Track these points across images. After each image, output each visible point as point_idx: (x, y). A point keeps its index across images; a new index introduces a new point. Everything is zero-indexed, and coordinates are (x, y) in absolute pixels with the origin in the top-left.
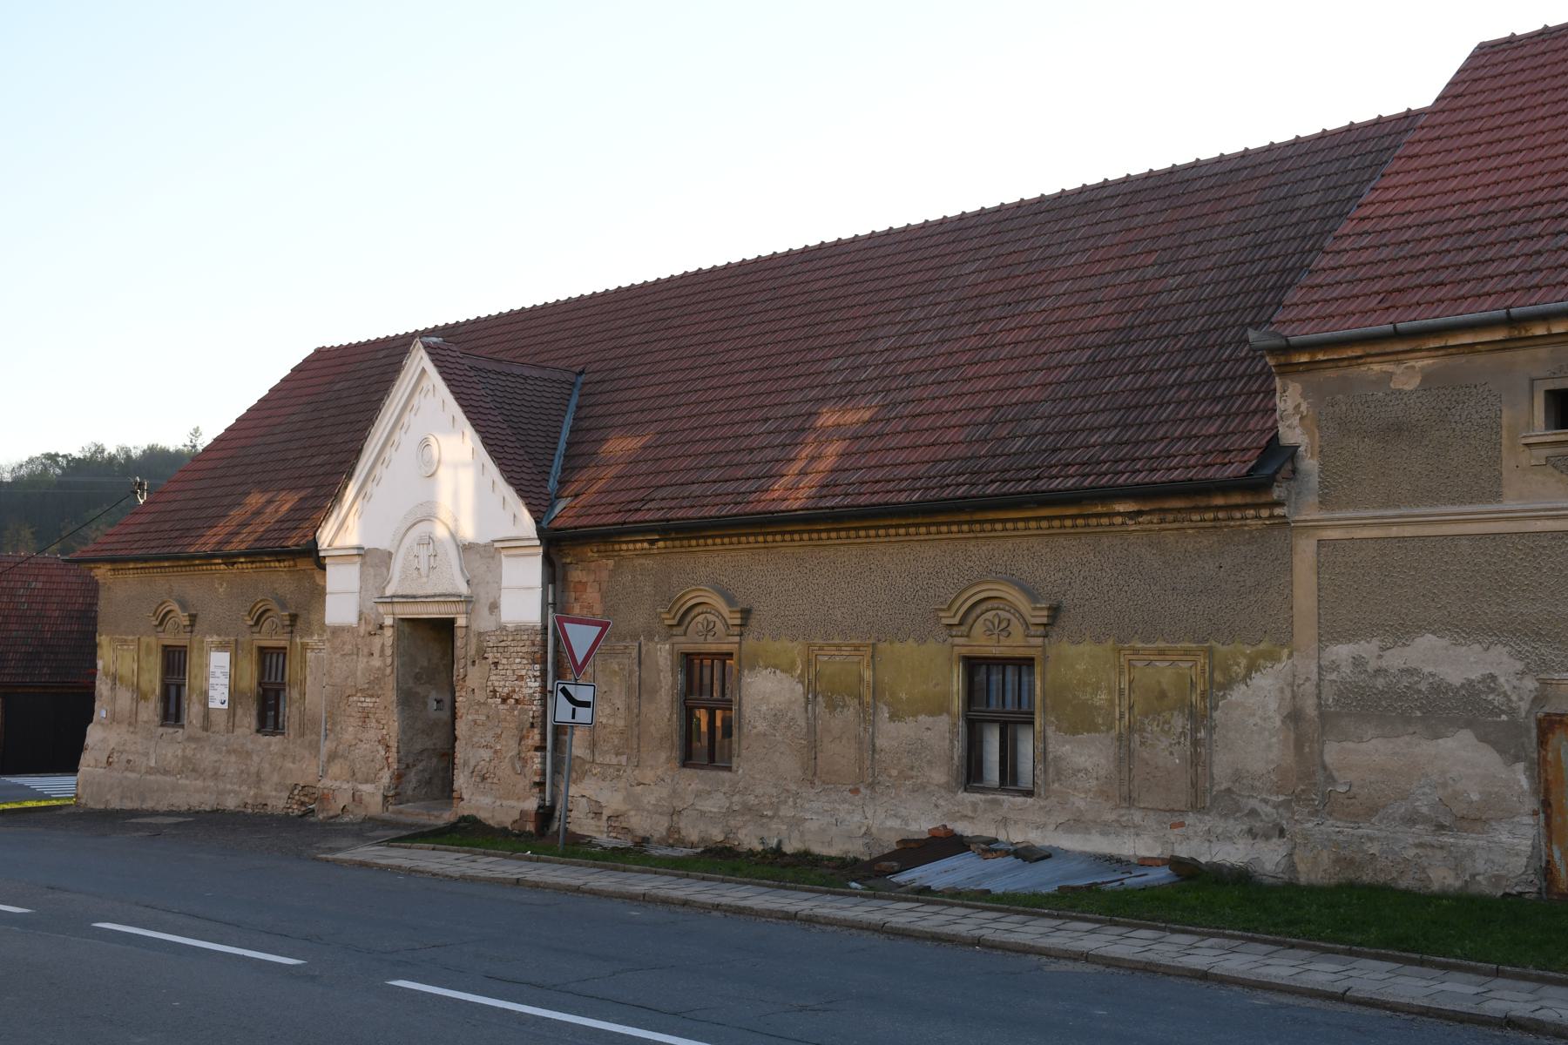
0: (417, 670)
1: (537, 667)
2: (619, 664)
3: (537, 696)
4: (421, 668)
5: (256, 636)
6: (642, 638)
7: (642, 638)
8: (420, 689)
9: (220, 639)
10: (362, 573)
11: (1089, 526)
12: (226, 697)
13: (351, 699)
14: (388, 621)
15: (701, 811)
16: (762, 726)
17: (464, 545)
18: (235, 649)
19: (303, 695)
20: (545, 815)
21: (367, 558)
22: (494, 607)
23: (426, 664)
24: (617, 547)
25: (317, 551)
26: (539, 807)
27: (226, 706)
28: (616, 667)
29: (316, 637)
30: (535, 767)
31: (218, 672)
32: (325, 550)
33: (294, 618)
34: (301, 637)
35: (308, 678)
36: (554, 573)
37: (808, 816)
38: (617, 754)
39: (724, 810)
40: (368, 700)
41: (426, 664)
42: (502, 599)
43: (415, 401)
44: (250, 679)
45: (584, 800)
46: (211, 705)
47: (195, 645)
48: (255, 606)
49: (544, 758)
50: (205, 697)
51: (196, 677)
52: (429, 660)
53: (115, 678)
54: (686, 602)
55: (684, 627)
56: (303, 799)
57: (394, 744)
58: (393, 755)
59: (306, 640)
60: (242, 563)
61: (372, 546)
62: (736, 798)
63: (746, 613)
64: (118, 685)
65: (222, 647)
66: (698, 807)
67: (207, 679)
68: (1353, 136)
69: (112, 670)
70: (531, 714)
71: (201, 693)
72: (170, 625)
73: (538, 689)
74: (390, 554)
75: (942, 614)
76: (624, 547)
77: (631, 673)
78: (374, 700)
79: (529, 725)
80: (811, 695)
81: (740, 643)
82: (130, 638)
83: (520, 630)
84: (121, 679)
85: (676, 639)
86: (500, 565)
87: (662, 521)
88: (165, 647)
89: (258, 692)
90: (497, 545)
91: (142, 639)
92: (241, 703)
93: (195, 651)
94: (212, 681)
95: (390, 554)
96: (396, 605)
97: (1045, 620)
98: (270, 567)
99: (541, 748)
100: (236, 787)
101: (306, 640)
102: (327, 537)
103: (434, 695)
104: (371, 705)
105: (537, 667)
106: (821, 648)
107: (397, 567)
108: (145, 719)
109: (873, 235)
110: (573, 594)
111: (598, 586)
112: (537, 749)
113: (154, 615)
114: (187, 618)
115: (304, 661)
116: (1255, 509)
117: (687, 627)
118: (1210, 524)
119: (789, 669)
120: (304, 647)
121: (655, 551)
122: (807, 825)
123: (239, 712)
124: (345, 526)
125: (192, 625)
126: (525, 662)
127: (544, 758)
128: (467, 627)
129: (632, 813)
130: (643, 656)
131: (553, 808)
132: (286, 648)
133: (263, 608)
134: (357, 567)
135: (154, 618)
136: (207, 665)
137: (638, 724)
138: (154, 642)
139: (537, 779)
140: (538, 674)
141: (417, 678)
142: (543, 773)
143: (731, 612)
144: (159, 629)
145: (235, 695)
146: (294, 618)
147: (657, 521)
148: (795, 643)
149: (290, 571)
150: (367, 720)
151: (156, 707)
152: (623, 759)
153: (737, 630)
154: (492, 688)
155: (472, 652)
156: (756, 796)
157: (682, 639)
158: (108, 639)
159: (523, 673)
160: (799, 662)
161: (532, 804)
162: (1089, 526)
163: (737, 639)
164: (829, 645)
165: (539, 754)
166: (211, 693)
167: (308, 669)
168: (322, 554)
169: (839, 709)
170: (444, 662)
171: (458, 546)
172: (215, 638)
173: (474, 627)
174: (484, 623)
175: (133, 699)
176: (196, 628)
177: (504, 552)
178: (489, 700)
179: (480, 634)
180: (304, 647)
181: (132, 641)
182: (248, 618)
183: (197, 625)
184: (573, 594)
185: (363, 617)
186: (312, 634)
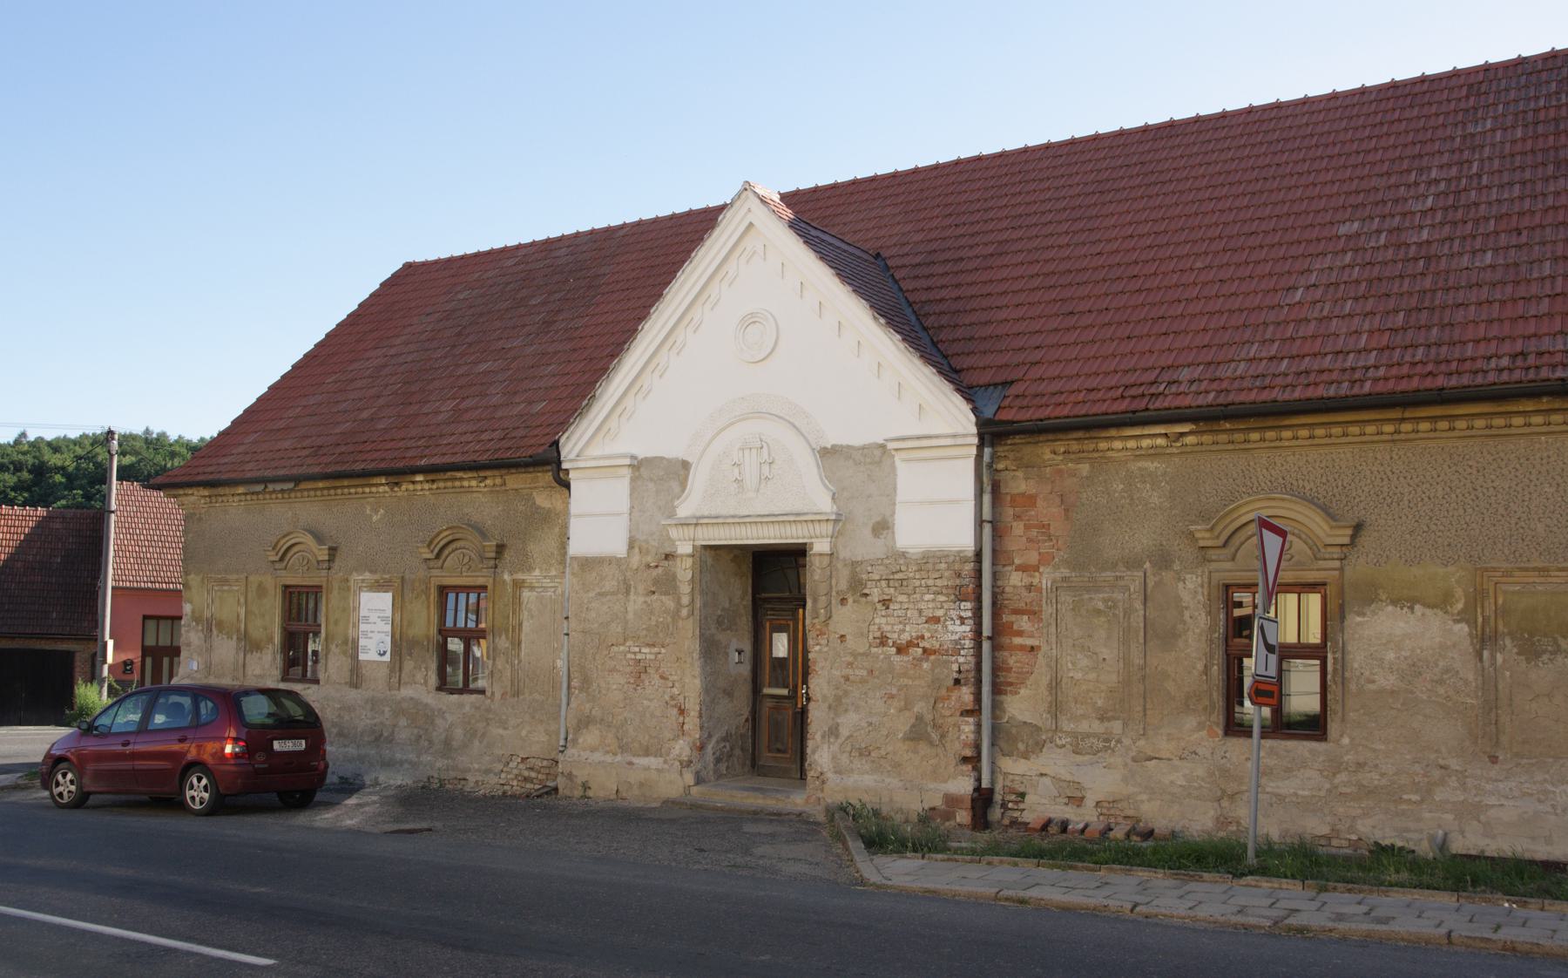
0: (719, 612)
1: (968, 605)
2: (1105, 601)
3: (968, 643)
4: (723, 609)
5: (435, 572)
6: (1147, 565)
7: (1147, 565)
8: (720, 637)
9: (377, 577)
10: (633, 490)
11: (1530, 425)
12: (388, 647)
13: (615, 649)
14: (685, 548)
15: (1277, 795)
16: (1386, 680)
17: (825, 448)
18: (401, 592)
19: (517, 644)
20: (982, 800)
21: (642, 470)
22: (883, 527)
23: (727, 605)
24: (1103, 445)
25: (559, 463)
26: (975, 790)
27: (387, 658)
28: (1100, 605)
29: (537, 572)
30: (963, 737)
31: (373, 617)
32: (571, 460)
33: (500, 549)
34: (511, 573)
35: (525, 624)
36: (990, 485)
37: (1492, 801)
38: (1102, 719)
39: (1322, 794)
40: (644, 650)
41: (727, 605)
42: (896, 516)
43: (731, 267)
44: (424, 623)
45: (1046, 780)
46: (362, 657)
47: (336, 585)
48: (438, 534)
49: (979, 725)
50: (352, 648)
51: (336, 622)
52: (731, 600)
53: (210, 626)
54: (1240, 516)
55: (1233, 550)
56: (526, 773)
57: (693, 706)
58: (692, 722)
59: (520, 576)
60: (421, 482)
61: (650, 454)
62: (1342, 777)
63: (333, 551)
64: (215, 632)
65: (378, 587)
66: (1268, 789)
67: (356, 626)
68: (1051, 152)
69: (207, 614)
70: (955, 667)
71: (346, 642)
72: (293, 559)
73: (970, 635)
74: (686, 465)
75: (268, 553)
76: (1118, 444)
77: (1128, 613)
78: (656, 650)
79: (952, 682)
80: (1485, 640)
81: (1341, 569)
82: (235, 576)
83: (929, 561)
84: (220, 625)
85: (1214, 566)
86: (893, 468)
87: (1127, 412)
88: (286, 587)
89: (438, 641)
90: (891, 446)
91: (251, 578)
92: (410, 655)
93: (335, 592)
94: (363, 627)
95: (686, 465)
96: (699, 528)
97: (1346, 540)
98: (462, 487)
99: (975, 711)
100: (412, 757)
101: (520, 576)
102: (577, 446)
103: (735, 644)
104: (652, 657)
105: (968, 605)
106: (1508, 573)
107: (698, 480)
108: (257, 672)
109: (640, 223)
110: (1010, 511)
111: (1058, 500)
112: (966, 713)
113: (274, 549)
114: (326, 552)
115: (517, 601)
116: (1525, 417)
117: (1237, 551)
118: (1389, 437)
119: (1442, 602)
120: (518, 585)
121: (1175, 450)
122: (1492, 813)
123: (409, 665)
124: (605, 429)
125: (331, 560)
126: (942, 598)
127: (979, 725)
128: (832, 554)
129: (1144, 797)
130: (1149, 590)
131: (991, 791)
132: (321, 587)
133: (450, 538)
134: (626, 481)
135: (273, 553)
136: (357, 609)
137: (1144, 678)
138: (272, 584)
139: (968, 753)
140: (969, 614)
141: (719, 622)
142: (977, 747)
143: (1332, 527)
144: (278, 566)
145: (401, 645)
146: (500, 549)
147: (1123, 413)
148: (1451, 569)
149: (492, 492)
150: (643, 676)
151: (275, 659)
152: (1117, 726)
153: (326, 565)
154: (878, 634)
155: (843, 585)
156: (1382, 775)
157: (1228, 565)
158: (199, 579)
159: (940, 613)
160: (1459, 592)
161: (963, 785)
162: (1530, 425)
163: (1337, 564)
164: (1521, 569)
165: (971, 720)
166: (362, 642)
167: (526, 613)
168: (564, 466)
169: (1545, 657)
170: (745, 603)
171: (813, 449)
172: (367, 575)
173: (844, 554)
174: (863, 547)
175: (238, 649)
176: (336, 565)
177: (904, 455)
178: (874, 650)
179: (854, 564)
180: (518, 585)
181: (237, 580)
182: (426, 550)
183: (337, 560)
184: (1010, 511)
185: (637, 545)
186: (530, 569)
